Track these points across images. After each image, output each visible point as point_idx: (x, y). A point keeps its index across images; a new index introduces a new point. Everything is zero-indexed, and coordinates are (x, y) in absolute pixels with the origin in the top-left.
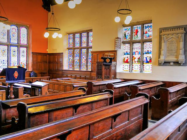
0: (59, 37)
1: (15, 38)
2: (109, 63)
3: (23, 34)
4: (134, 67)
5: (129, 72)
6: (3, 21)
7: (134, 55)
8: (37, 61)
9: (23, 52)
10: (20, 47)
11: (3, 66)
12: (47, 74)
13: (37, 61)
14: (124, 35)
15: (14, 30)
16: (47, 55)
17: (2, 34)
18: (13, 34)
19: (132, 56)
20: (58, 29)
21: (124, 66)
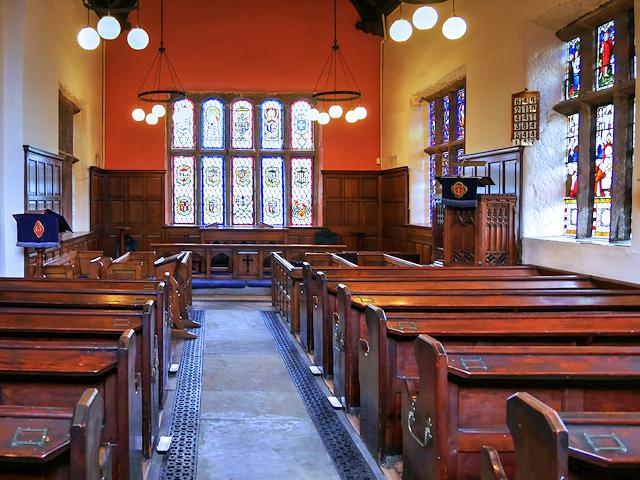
0: (149, 123)
1: (274, 134)
2: (465, 197)
3: (298, 122)
4: (598, 218)
5: (574, 241)
6: (164, 101)
7: (598, 162)
8: (340, 197)
9: (302, 172)
10: (294, 157)
11: (241, 212)
12: (380, 238)
13: (340, 197)
14: (567, 77)
15: (271, 112)
16: (380, 177)
17: (237, 127)
18: (269, 124)
19: (587, 169)
20: (352, 93)
21: (569, 211)
